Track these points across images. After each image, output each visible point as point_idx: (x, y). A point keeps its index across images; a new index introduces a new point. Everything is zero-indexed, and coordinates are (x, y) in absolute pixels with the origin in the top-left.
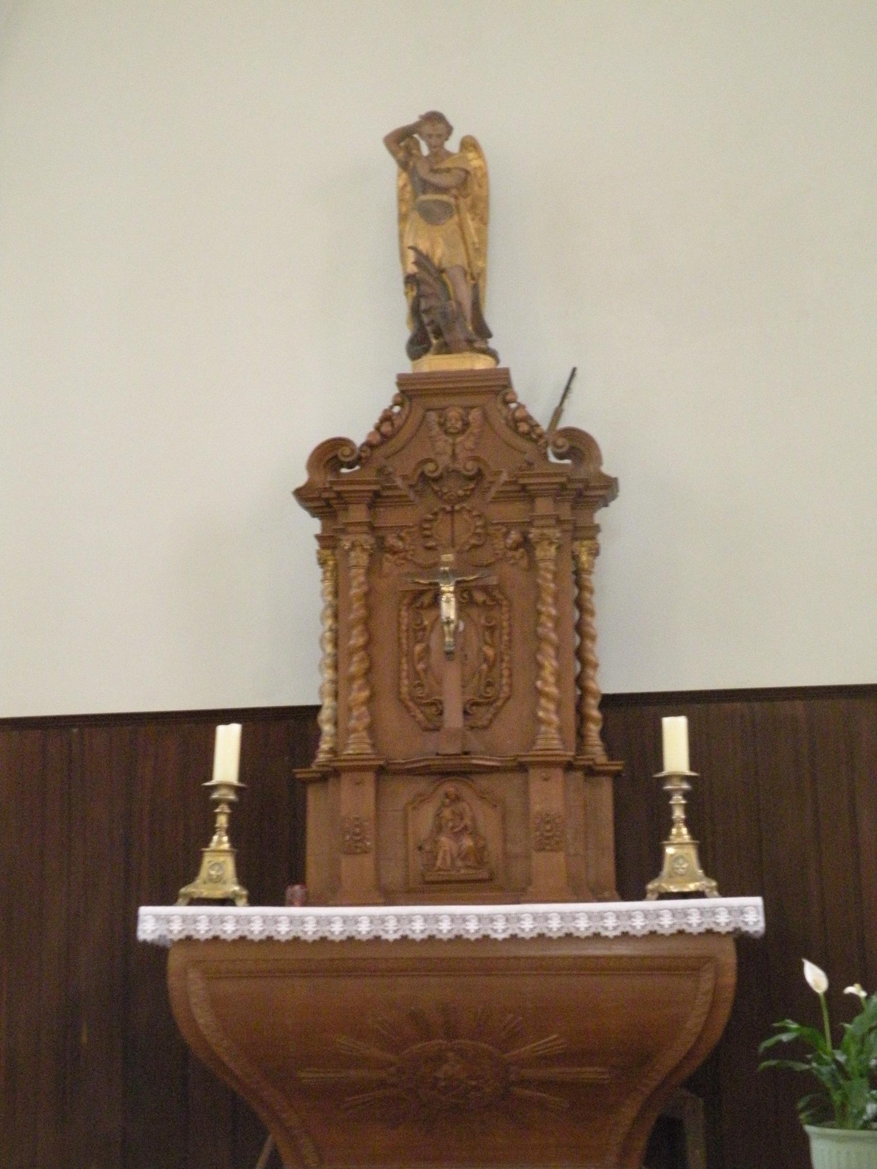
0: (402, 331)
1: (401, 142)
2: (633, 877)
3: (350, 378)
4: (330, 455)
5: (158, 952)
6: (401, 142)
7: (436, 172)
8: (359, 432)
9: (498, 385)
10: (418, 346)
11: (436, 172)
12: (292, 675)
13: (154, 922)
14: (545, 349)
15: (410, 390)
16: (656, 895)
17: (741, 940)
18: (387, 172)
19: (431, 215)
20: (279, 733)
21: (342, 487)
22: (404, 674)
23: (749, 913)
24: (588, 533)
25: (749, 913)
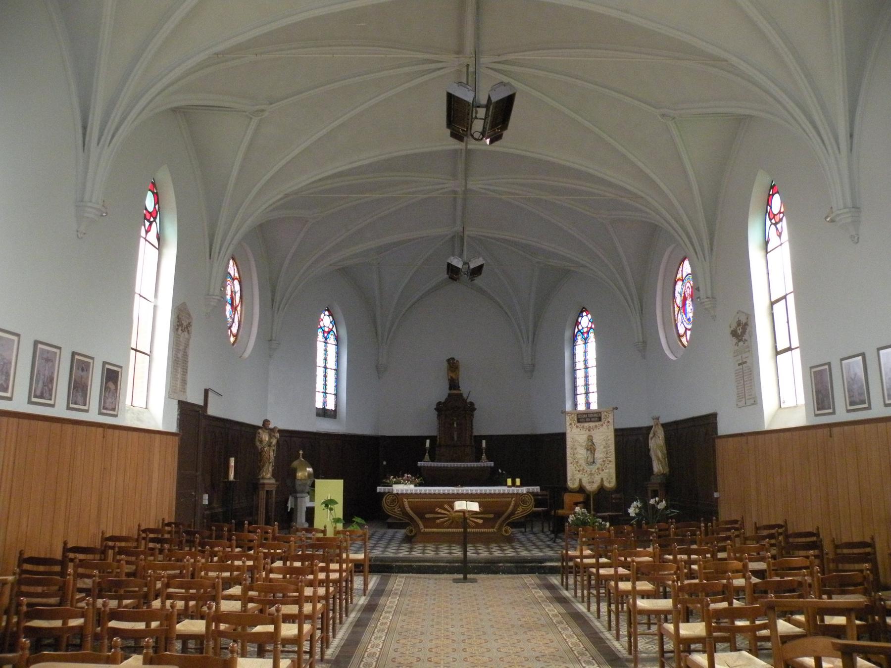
0: (448, 387)
1: (448, 360)
2: (478, 459)
3: (441, 392)
4: (439, 403)
5: (421, 467)
6: (448, 360)
7: (453, 365)
8: (443, 400)
9: (461, 395)
10: (450, 389)
11: (453, 365)
12: (434, 432)
13: (419, 464)
14: (469, 388)
15: (449, 395)
16: (111, 385)
17: (491, 467)
18: (446, 364)
19: (453, 371)
20: (433, 439)
21: (440, 408)
22: (353, 616)
23: (492, 464)
24: (473, 415)
25: (492, 464)
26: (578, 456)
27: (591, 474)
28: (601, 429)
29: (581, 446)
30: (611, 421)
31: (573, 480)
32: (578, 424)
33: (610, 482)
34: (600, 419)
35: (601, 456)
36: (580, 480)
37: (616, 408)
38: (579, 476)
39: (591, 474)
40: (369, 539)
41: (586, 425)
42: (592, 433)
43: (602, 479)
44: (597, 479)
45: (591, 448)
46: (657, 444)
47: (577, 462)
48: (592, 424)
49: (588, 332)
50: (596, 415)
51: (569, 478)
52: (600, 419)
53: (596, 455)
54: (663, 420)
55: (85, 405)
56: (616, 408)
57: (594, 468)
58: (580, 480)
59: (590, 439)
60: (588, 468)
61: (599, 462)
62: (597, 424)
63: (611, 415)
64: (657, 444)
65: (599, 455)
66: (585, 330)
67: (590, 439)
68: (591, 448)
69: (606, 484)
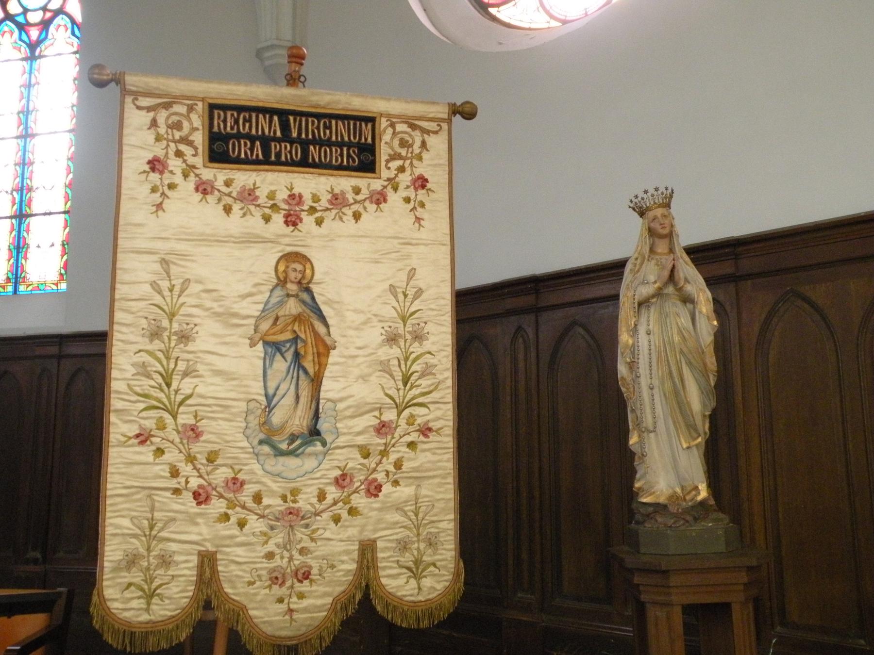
26: (207, 387)
27: (292, 516)
28: (371, 217)
29: (227, 317)
30: (437, 179)
31: (148, 564)
32: (218, 175)
33: (416, 570)
34: (365, 161)
35: (371, 391)
36: (207, 563)
37: (467, 112)
38: (193, 531)
39: (292, 516)
40: (128, 385)
41: (274, 182)
42: (310, 237)
43: (367, 552)
44: (334, 553)
45: (297, 335)
46: (664, 359)
47: (194, 432)
48: (310, 184)
49: (45, 25)
50: (341, 131)
51: (112, 552)
52: (365, 161)
53: (330, 388)
54: (698, 225)
55: (725, 608)
56: (467, 112)
57: (312, 472)
58: (207, 563)
59: (295, 275)
60: (266, 476)
61: (349, 431)
62: (345, 183)
63: (438, 143)
64: (664, 359)
65: (352, 383)
66: (35, 17)
67: (295, 275)
68: (297, 335)
69: (398, 584)
